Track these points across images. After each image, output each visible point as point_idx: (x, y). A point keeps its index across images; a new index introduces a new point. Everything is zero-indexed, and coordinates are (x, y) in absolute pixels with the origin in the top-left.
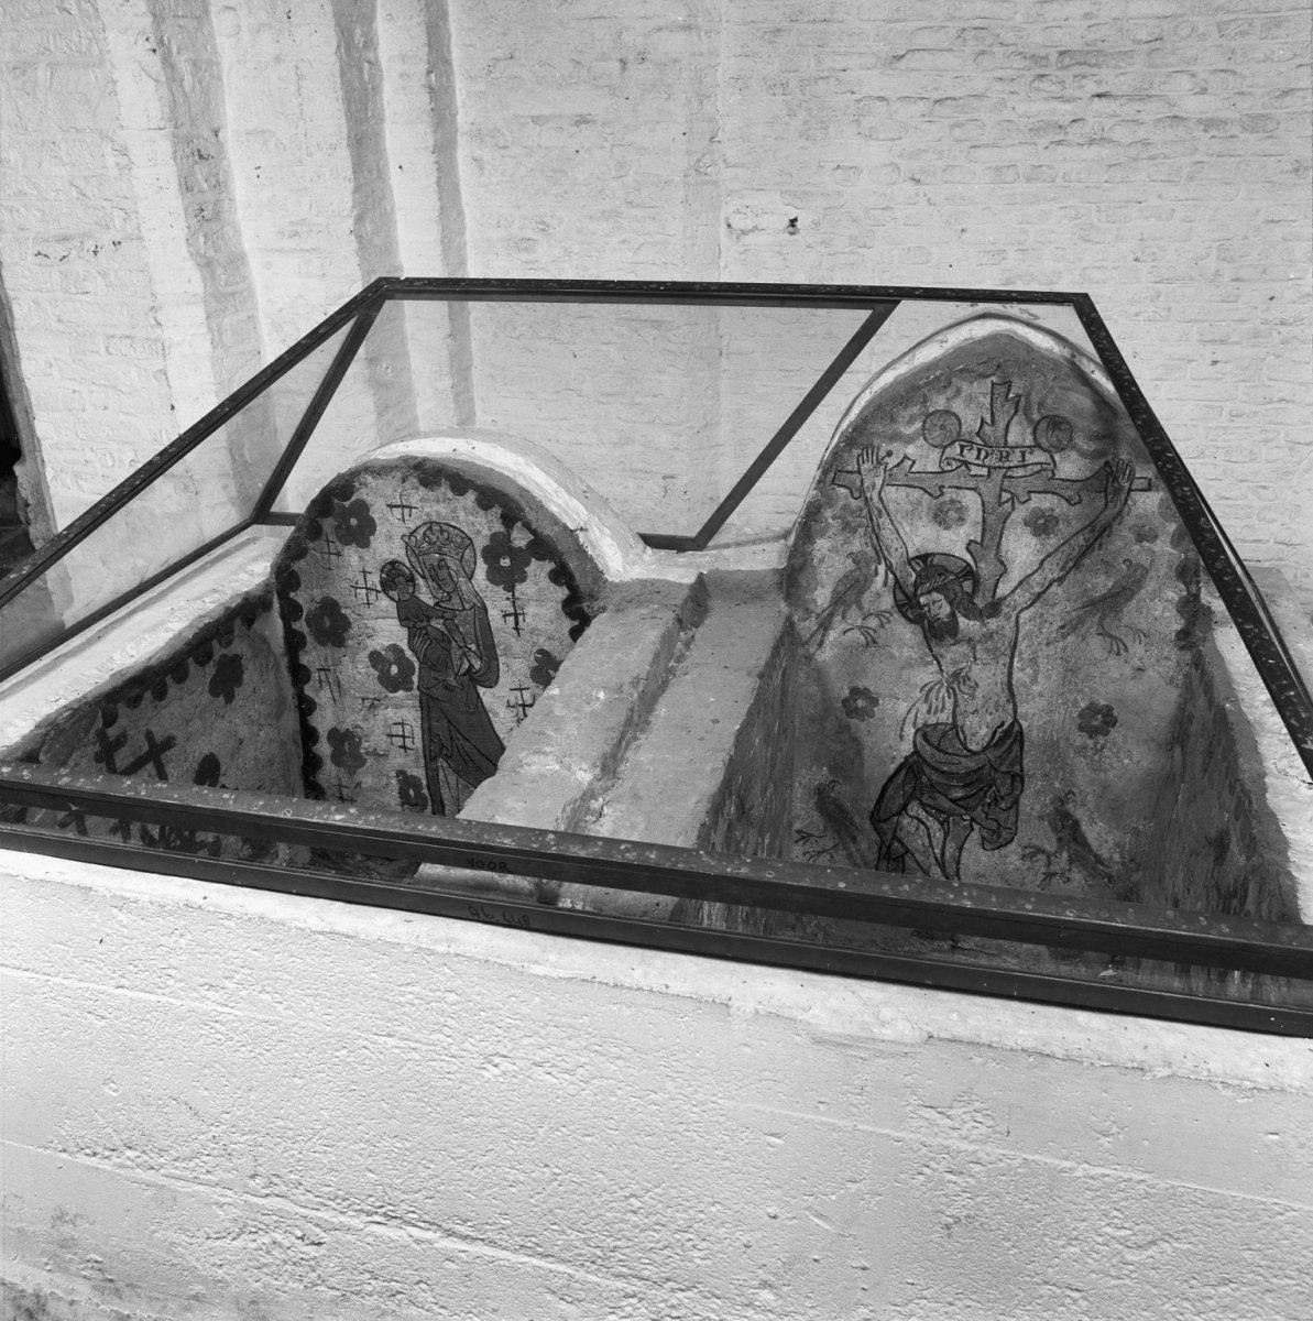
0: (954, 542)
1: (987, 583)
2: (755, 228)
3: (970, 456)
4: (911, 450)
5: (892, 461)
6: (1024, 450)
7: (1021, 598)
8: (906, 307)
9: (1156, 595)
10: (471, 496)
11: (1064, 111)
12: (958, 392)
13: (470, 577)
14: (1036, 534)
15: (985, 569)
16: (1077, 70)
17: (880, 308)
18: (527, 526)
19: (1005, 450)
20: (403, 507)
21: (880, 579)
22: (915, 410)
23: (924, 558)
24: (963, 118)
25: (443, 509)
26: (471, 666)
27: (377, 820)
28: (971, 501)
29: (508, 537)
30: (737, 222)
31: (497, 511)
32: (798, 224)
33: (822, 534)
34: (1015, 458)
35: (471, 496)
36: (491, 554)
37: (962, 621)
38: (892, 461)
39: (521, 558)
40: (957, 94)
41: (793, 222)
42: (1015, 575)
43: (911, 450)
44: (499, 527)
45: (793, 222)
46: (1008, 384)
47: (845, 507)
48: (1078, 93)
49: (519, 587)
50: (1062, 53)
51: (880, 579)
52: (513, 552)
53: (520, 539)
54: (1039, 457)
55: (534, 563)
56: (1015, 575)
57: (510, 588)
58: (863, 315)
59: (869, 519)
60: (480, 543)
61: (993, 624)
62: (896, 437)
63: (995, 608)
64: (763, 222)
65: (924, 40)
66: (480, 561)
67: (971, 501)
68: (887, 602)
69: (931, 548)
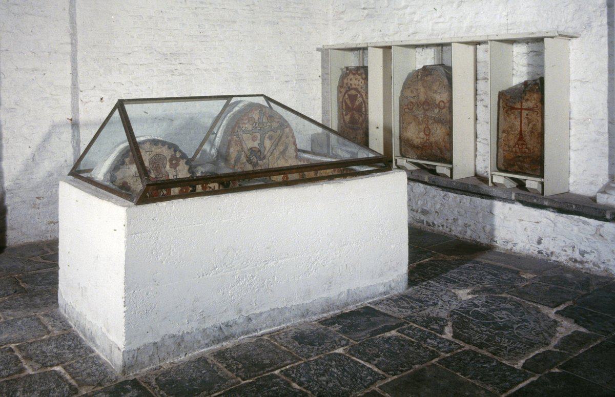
0: (256, 144)
1: (262, 152)
2: (90, 101)
3: (257, 126)
4: (247, 126)
5: (243, 129)
6: (267, 123)
7: (269, 154)
8: (234, 98)
9: (291, 148)
10: (166, 146)
11: (173, 67)
12: (254, 113)
13: (165, 168)
14: (270, 140)
15: (262, 150)
16: (175, 57)
17: (229, 99)
18: (180, 151)
19: (263, 123)
20: (149, 151)
21: (243, 156)
22: (246, 117)
23: (251, 149)
24: (148, 69)
25: (159, 150)
26: (163, 193)
27: (277, 179)
28: (258, 135)
29: (175, 155)
30: (84, 100)
31: (173, 149)
32: (103, 99)
33: (232, 147)
34: (265, 125)
35: (166, 146)
36: (171, 160)
37: (259, 162)
38: (243, 129)
39: (178, 160)
40: (146, 63)
41: (101, 99)
42: (267, 149)
43: (247, 126)
44: (173, 153)
45: (101, 99)
46: (262, 110)
47: (236, 140)
48: (175, 63)
49: (177, 168)
50: (170, 53)
51: (243, 156)
52: (176, 159)
53: (178, 155)
54: (269, 124)
55: (182, 160)
56: (267, 149)
57: (175, 169)
58: (225, 101)
59: (240, 142)
60: (168, 158)
61: (264, 161)
62: (244, 123)
63: (264, 157)
64: (92, 99)
65: (136, 49)
66: (168, 162)
67: (258, 135)
68: (245, 160)
69: (252, 146)
